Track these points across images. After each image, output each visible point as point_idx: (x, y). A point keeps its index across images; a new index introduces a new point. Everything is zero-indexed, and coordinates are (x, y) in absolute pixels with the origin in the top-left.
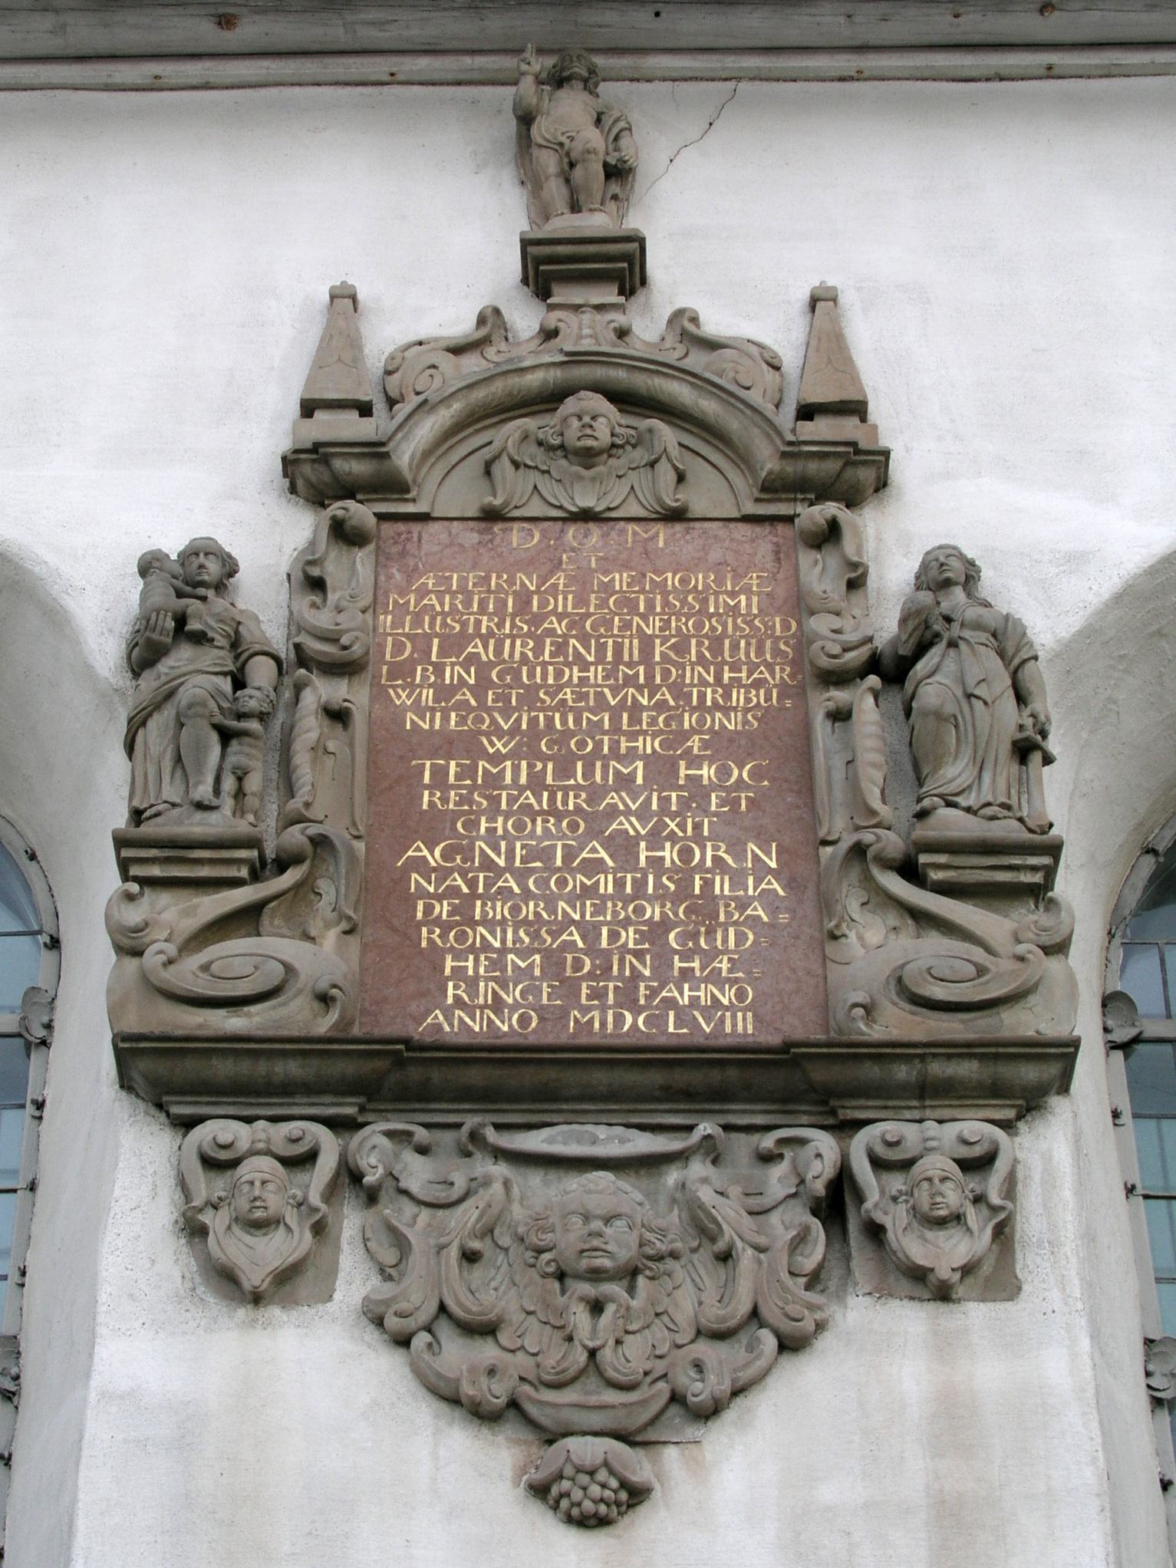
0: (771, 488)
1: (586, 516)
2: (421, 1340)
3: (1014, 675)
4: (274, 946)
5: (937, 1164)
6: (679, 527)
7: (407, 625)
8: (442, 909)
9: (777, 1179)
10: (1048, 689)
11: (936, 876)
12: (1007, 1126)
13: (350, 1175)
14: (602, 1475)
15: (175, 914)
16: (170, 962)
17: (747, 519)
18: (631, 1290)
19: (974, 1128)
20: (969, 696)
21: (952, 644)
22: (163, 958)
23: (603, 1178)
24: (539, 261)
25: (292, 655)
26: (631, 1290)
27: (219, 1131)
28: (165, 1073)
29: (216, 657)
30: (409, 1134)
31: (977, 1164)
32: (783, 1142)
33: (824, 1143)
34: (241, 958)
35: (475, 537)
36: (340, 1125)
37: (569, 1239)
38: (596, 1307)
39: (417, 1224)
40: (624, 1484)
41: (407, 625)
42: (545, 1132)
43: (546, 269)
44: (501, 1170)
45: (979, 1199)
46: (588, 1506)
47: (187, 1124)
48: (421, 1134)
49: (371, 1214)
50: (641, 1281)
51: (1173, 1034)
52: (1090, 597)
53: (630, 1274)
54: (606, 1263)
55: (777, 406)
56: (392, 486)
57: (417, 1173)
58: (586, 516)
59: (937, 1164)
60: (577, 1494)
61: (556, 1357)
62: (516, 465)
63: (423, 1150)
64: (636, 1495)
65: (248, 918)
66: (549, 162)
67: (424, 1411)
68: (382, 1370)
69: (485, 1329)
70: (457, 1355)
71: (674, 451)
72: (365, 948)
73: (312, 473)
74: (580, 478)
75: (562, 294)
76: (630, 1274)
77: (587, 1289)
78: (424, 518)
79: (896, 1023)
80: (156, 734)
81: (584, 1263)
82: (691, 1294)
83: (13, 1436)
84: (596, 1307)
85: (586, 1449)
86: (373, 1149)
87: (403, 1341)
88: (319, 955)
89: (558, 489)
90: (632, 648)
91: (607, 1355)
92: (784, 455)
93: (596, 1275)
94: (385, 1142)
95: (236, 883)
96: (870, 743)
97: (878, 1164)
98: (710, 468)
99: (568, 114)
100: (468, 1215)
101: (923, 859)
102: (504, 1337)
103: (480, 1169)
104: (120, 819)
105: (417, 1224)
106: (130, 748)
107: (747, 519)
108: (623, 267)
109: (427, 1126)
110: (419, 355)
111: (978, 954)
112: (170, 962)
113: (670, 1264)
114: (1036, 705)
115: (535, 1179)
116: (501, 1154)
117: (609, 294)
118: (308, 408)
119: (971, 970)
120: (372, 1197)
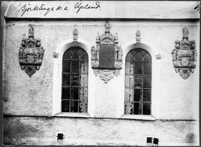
19: (119, 71)
27: (95, 70)
31: (118, 72)
39: (101, 73)
44: (103, 72)
51: (198, 17)
53: (107, 75)
55: (128, 133)
57: (101, 71)
61: (105, 78)
66: (106, 27)
67: (175, 46)
69: (103, 77)
76: (107, 75)
80: (92, 54)
82: (110, 76)
85: (106, 81)
86: (99, 70)
99: (107, 25)
105: (101, 73)
116: (104, 71)
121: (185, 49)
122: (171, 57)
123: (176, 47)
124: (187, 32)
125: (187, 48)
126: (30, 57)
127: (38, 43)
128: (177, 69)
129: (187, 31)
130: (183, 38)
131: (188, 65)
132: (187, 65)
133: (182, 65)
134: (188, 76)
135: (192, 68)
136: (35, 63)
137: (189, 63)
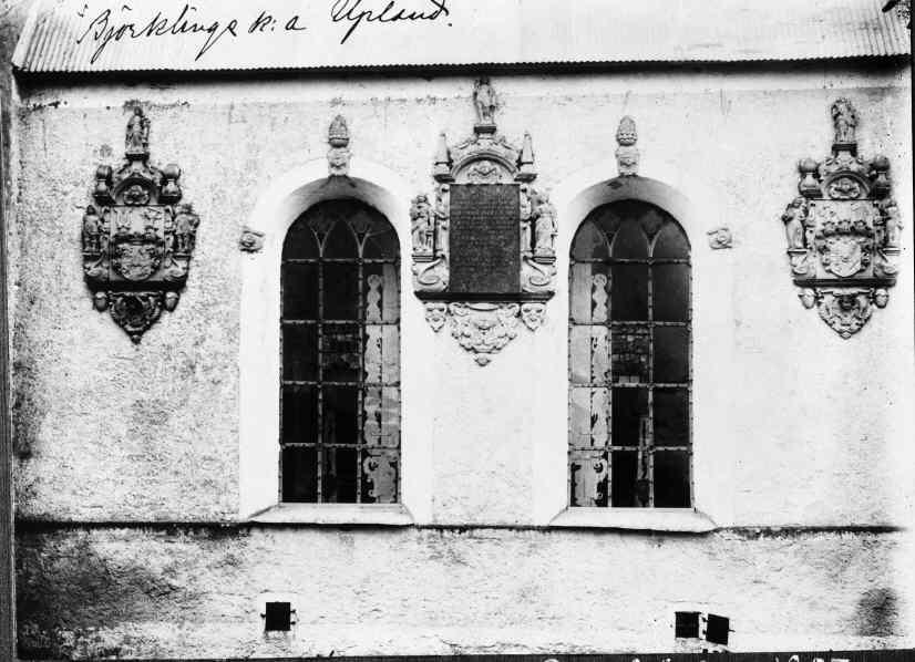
5: (533, 312)
7: (616, 448)
10: (407, 244)
13: (449, 311)
15: (422, 267)
28: (423, 296)
31: (539, 311)
33: (517, 306)
41: (616, 448)
52: (633, 193)
53: (488, 329)
57: (458, 311)
59: (533, 312)
61: (479, 341)
66: (480, 106)
70: (465, 341)
80: (416, 233)
82: (499, 331)
86: (452, 306)
98: (290, 535)
100: (467, 318)
105: (458, 319)
121: (844, 200)
122: (777, 240)
123: (801, 193)
124: (850, 121)
125: (854, 195)
126: (133, 250)
127: (171, 187)
128: (809, 292)
129: (853, 117)
130: (836, 149)
131: (861, 271)
132: (853, 271)
133: (830, 271)
134: (862, 325)
135: (877, 287)
136: (158, 278)
137: (865, 264)
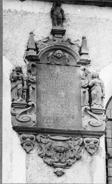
0: (78, 63)
1: (58, 65)
2: (44, 157)
3: (102, 88)
4: (28, 115)
5: (92, 143)
6: (68, 66)
8: (44, 111)
9: (76, 143)
11: (93, 112)
12: (98, 138)
13: (37, 140)
14: (61, 172)
16: (19, 117)
17: (75, 66)
18: (63, 153)
20: (98, 92)
21: (96, 86)
22: (18, 117)
23: (61, 142)
24: (54, 31)
25: (20, 96)
26: (63, 153)
27: (24, 135)
29: (21, 81)
30: (42, 136)
31: (95, 143)
32: (78, 139)
33: (81, 139)
34: (25, 118)
35: (46, 66)
36: (36, 135)
37: (58, 149)
38: (60, 155)
40: (63, 172)
42: (55, 137)
43: (53, 32)
44: (51, 141)
45: (96, 146)
46: (60, 175)
47: (21, 134)
48: (43, 136)
49: (38, 144)
50: (64, 153)
53: (63, 152)
54: (61, 151)
56: (39, 60)
57: (43, 140)
58: (58, 65)
59: (92, 143)
60: (58, 173)
62: (51, 58)
63: (43, 138)
64: (64, 173)
65: (25, 112)
68: (41, 160)
69: (50, 157)
71: (68, 57)
72: (37, 115)
73: (29, 58)
74: (58, 60)
75: (56, 36)
77: (59, 154)
78: (41, 63)
79: (89, 129)
81: (60, 151)
83: (45, 52)
84: (60, 155)
85: (60, 169)
87: (42, 157)
88: (33, 116)
89: (55, 61)
90: (63, 82)
91: (61, 160)
92: (80, 60)
93: (60, 152)
94: (40, 137)
95: (24, 108)
96: (87, 96)
97: (86, 142)
101: (92, 110)
102: (52, 158)
103: (50, 154)
104: (10, 103)
105: (43, 146)
106: (12, 91)
107: (75, 66)
108: (63, 32)
109: (43, 135)
110: (40, 43)
111: (97, 121)
112: (19, 117)
113: (67, 151)
114: (103, 92)
115: (54, 142)
117: (61, 36)
118: (28, 50)
119: (96, 123)
120: (38, 142)
